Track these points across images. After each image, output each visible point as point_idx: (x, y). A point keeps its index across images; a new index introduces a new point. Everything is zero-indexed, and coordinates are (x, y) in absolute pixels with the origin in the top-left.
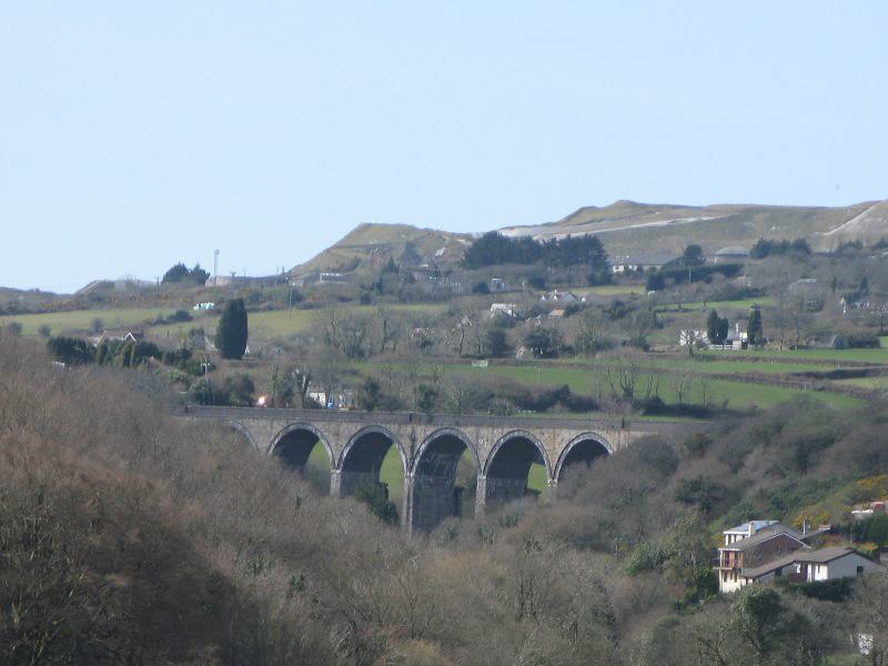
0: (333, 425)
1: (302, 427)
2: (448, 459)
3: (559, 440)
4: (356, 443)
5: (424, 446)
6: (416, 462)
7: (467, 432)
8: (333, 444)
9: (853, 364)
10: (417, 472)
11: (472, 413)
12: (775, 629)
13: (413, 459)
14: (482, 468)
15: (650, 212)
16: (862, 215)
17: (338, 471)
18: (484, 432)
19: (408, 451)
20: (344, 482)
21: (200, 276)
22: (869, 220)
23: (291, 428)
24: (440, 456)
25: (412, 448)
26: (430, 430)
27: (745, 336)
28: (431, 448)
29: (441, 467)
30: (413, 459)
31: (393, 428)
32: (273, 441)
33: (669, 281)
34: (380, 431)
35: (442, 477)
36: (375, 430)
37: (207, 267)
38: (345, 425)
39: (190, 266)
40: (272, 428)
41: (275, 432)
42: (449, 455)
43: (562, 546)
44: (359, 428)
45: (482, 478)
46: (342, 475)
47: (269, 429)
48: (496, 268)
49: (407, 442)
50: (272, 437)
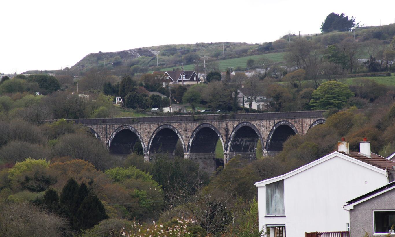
1: (166, 127)
2: (251, 141)
4: (196, 134)
5: (233, 134)
8: (183, 137)
10: (230, 151)
11: (40, 179)
12: (24, 207)
13: (227, 142)
14: (265, 146)
17: (188, 153)
19: (224, 138)
22: (334, 47)
24: (245, 140)
25: (227, 135)
26: (236, 123)
28: (237, 135)
32: (151, 137)
34: (209, 126)
35: (248, 153)
38: (190, 124)
40: (150, 129)
41: (152, 131)
42: (250, 139)
43: (119, 198)
44: (198, 125)
47: (149, 130)
49: (223, 132)
50: (151, 134)
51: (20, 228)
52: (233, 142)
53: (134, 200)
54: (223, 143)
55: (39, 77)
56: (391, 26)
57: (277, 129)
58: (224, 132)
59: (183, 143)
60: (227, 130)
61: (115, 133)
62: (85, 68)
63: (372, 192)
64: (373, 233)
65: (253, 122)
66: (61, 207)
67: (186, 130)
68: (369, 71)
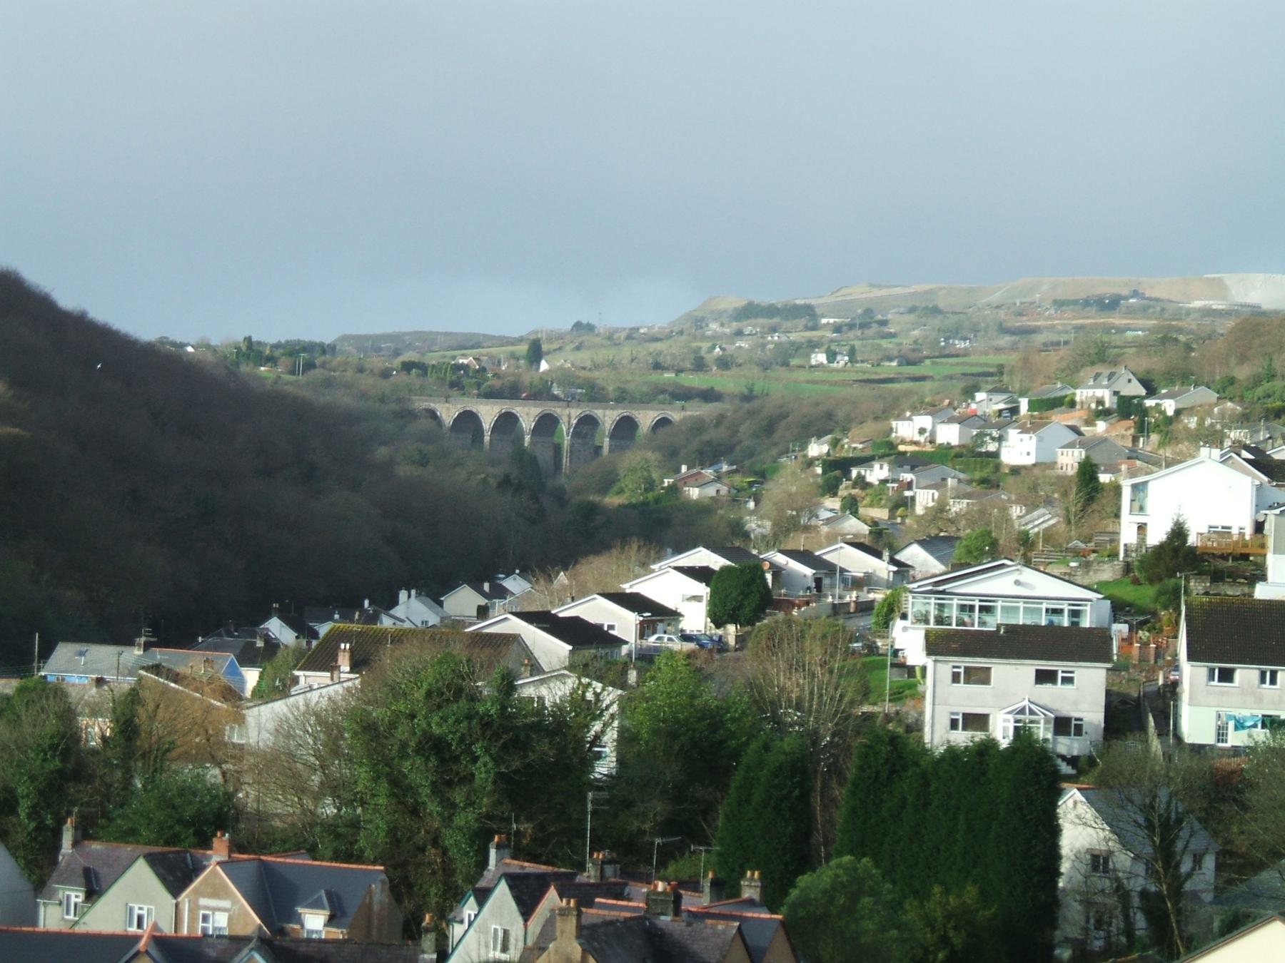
0: (526, 409)
3: (648, 417)
5: (575, 422)
6: (571, 430)
7: (598, 413)
9: (987, 365)
13: (569, 429)
15: (507, 342)
16: (1002, 291)
18: (608, 412)
19: (567, 424)
20: (611, 446)
21: (590, 328)
23: (503, 411)
25: (569, 422)
27: (847, 358)
29: (586, 434)
30: (569, 429)
31: (558, 410)
33: (845, 328)
36: (548, 412)
37: (594, 321)
39: (585, 322)
41: (494, 413)
45: (607, 440)
46: (531, 438)
48: (753, 321)
51: (470, 818)
52: (575, 428)
53: (496, 673)
54: (564, 429)
55: (462, 388)
56: (1282, 601)
57: (620, 420)
58: (567, 419)
59: (524, 426)
60: (569, 417)
61: (457, 413)
62: (1253, 570)
63: (494, 336)
64: (917, 480)
65: (596, 411)
66: (989, 529)
67: (528, 414)
68: (1028, 512)
